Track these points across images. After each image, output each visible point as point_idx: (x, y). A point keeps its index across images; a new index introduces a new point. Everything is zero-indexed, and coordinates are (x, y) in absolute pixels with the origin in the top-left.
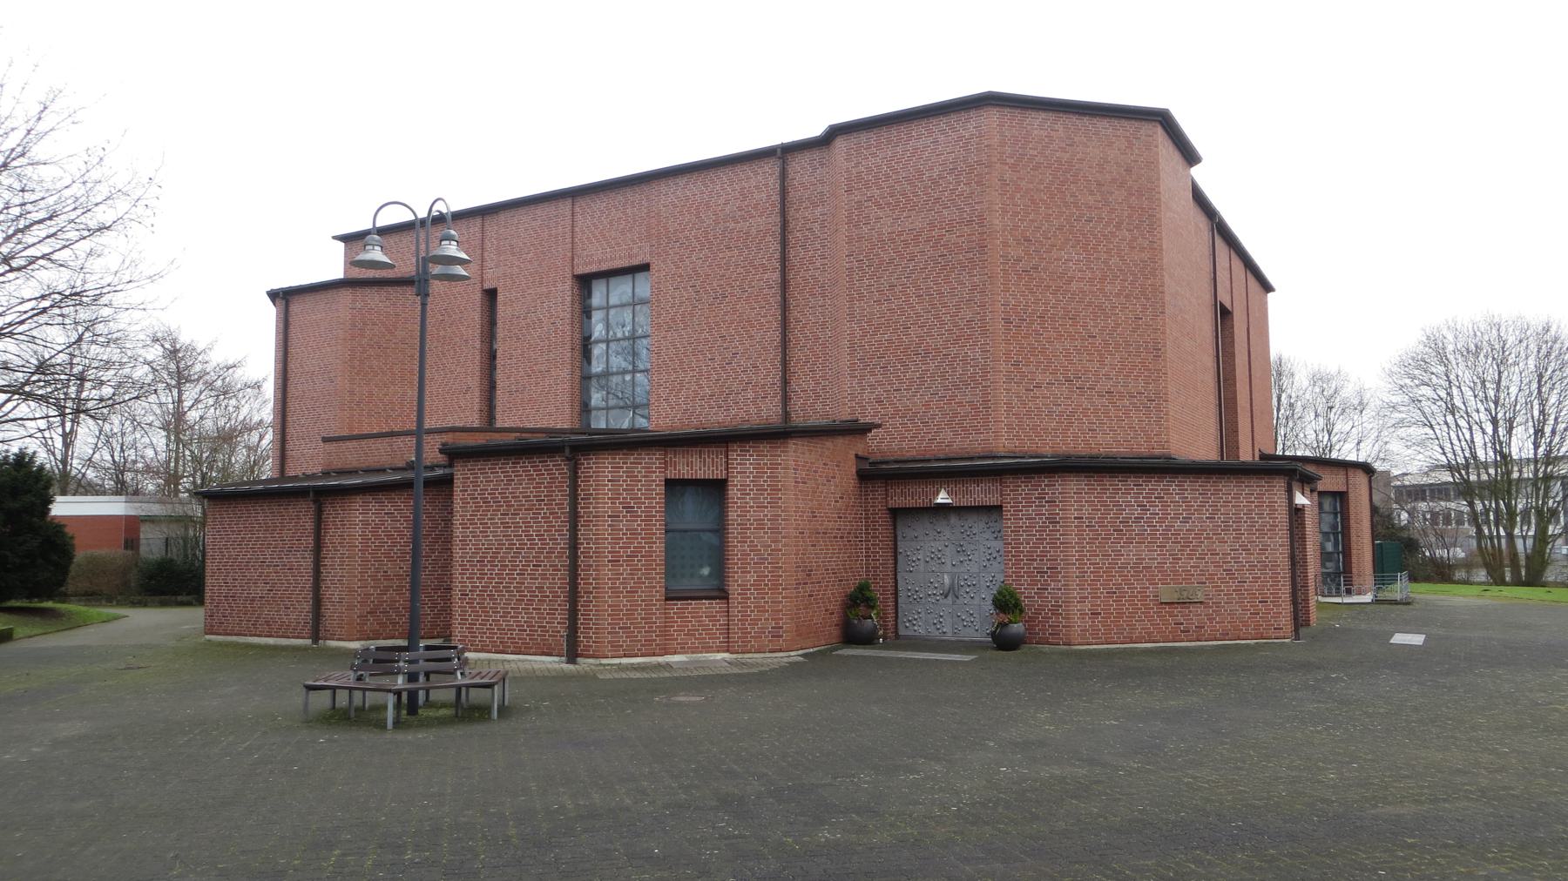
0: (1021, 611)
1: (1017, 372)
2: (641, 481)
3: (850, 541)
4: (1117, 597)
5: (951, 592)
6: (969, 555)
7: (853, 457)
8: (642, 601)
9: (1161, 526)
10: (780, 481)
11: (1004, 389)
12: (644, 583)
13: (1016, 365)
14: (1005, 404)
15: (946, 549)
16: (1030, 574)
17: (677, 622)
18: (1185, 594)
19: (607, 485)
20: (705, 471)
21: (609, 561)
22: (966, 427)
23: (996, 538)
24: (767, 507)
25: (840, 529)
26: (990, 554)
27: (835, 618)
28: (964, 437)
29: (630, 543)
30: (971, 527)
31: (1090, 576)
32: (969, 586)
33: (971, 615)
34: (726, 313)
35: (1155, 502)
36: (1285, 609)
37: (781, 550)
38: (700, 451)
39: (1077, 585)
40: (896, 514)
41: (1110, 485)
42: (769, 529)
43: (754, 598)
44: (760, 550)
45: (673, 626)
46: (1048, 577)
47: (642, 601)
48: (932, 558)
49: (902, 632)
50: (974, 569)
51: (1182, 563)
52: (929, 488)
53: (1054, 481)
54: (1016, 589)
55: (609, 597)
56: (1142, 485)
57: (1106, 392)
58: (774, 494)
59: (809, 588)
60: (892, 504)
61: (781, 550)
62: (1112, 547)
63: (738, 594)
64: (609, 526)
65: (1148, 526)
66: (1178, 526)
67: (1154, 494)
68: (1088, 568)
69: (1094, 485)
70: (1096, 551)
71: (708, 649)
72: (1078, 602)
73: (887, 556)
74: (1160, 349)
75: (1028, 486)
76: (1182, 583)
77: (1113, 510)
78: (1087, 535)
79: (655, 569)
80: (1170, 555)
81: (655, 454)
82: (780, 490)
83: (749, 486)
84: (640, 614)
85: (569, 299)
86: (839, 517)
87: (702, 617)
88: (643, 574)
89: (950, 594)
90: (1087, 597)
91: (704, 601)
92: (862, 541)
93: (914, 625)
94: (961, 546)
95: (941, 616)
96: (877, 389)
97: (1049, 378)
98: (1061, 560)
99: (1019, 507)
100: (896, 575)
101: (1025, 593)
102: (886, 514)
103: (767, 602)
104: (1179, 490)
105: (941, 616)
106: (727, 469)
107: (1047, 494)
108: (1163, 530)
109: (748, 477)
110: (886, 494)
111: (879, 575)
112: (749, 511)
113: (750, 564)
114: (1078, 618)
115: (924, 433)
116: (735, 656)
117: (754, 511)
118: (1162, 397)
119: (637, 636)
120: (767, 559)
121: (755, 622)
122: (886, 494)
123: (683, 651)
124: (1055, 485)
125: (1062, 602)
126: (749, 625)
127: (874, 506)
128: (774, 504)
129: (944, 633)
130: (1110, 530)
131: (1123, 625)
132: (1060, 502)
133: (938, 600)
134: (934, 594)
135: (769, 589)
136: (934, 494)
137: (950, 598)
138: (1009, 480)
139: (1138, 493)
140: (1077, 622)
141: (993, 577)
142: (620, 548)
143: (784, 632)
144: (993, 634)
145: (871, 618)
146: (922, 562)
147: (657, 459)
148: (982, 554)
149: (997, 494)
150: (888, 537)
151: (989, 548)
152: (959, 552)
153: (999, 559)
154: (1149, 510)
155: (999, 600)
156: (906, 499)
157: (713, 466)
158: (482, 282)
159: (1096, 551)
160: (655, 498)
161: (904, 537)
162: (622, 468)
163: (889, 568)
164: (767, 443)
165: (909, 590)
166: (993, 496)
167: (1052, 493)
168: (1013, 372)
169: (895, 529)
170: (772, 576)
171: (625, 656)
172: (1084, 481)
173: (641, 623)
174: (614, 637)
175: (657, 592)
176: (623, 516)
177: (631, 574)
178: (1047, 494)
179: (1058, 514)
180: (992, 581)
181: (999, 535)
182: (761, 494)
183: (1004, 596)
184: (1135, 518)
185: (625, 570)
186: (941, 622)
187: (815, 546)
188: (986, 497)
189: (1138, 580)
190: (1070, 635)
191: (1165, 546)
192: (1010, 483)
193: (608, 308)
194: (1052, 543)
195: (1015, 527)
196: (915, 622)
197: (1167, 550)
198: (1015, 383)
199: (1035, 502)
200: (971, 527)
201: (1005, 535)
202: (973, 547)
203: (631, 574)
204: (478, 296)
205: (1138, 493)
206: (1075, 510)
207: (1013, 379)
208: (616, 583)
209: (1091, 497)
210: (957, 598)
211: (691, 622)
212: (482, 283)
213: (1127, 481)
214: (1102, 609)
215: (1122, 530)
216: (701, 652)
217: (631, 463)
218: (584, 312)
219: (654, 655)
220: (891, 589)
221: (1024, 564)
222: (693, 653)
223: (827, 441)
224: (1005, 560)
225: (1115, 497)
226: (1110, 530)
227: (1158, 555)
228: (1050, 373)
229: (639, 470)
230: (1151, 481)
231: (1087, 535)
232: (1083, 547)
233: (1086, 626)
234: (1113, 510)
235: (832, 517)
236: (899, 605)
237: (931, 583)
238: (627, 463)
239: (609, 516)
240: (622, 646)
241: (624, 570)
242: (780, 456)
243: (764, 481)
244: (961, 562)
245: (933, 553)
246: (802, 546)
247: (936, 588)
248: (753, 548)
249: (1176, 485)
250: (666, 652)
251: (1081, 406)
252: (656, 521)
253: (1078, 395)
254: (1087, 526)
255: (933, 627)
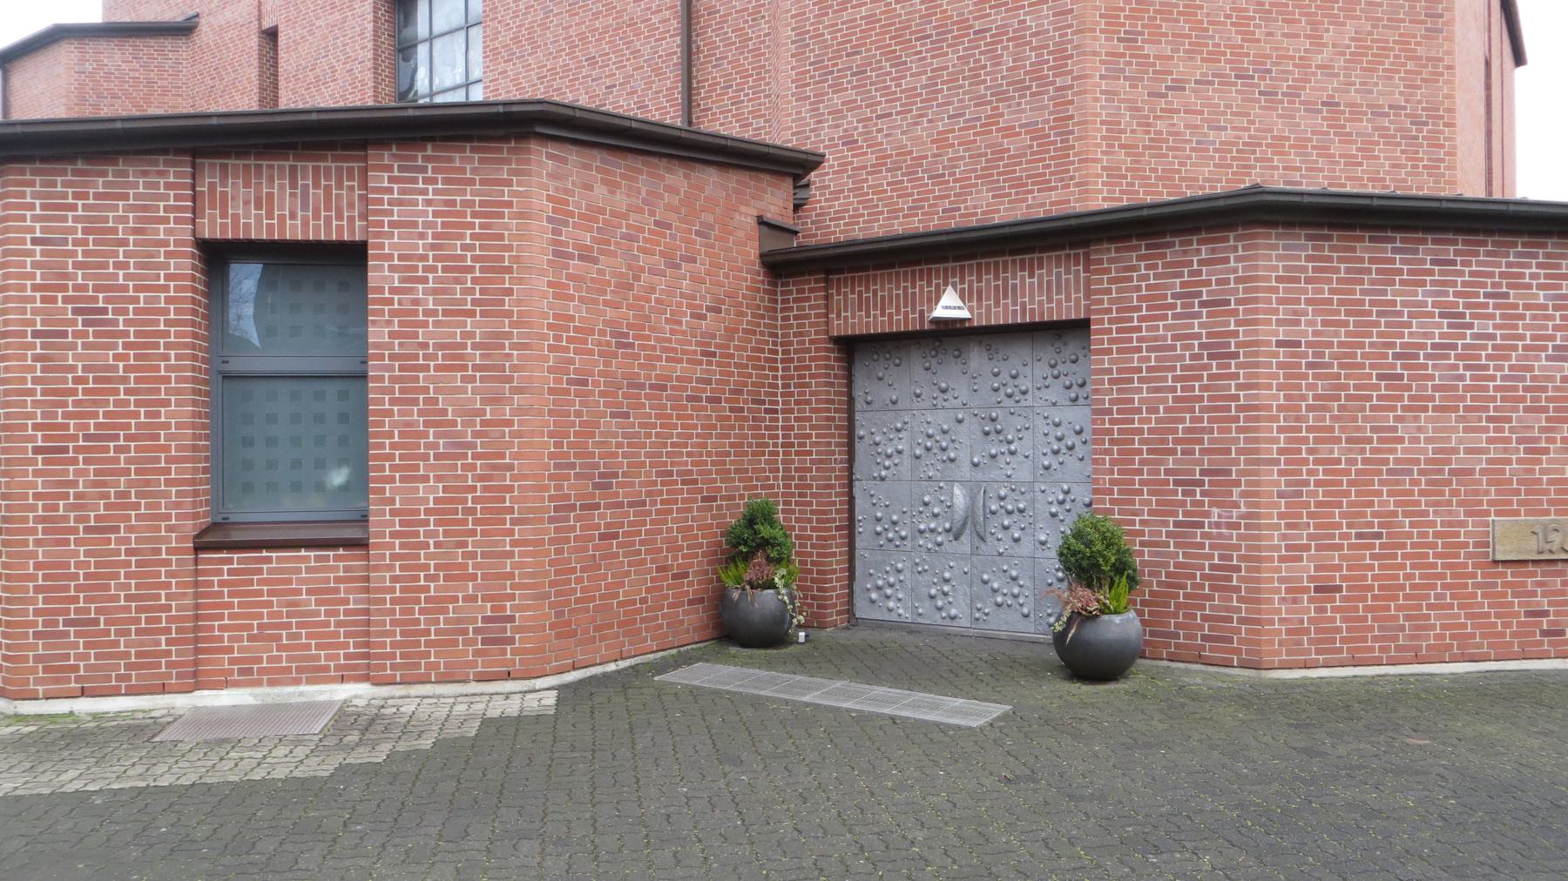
0: (1132, 581)
1: (1131, 56)
2: (124, 243)
3: (741, 410)
4: (1382, 546)
5: (968, 527)
6: (1010, 442)
7: (751, 222)
8: (129, 552)
9: (1499, 368)
10: (509, 248)
11: (1102, 92)
12: (136, 506)
13: (1130, 39)
14: (1103, 123)
15: (960, 427)
16: (1157, 487)
17: (230, 605)
18: (1557, 539)
19: (31, 253)
20: (328, 220)
21: (37, 450)
22: (1020, 178)
23: (1075, 400)
24: (471, 314)
25: (709, 382)
26: (1060, 439)
27: (692, 586)
28: (1016, 201)
29: (95, 403)
30: (1014, 377)
31: (1314, 494)
32: (1010, 513)
33: (1014, 579)
34: (596, 15)
35: (1486, 306)
36: (383, 391)
37: (510, 423)
38: (293, 170)
39: (1281, 516)
40: (851, 348)
41: (1372, 261)
42: (476, 368)
43: (438, 545)
44: (454, 423)
45: (220, 617)
46: (1204, 494)
47: (129, 552)
48: (928, 449)
49: (862, 610)
50: (1023, 474)
51: (1550, 461)
52: (921, 287)
53: (1226, 250)
54: (1119, 522)
55: (38, 543)
56: (1453, 263)
57: (1324, 104)
58: (489, 281)
59: (603, 518)
60: (839, 327)
61: (510, 423)
62: (1374, 419)
63: (394, 535)
64: (36, 358)
65: (1467, 368)
66: (1542, 368)
67: (1484, 285)
68: (1311, 472)
69: (1330, 259)
70: (1331, 429)
71: (318, 675)
72: (1282, 559)
73: (829, 444)
74: (1441, 16)
75: (1155, 267)
76: (1547, 513)
77: (1377, 324)
78: (1310, 387)
79: (167, 471)
80: (1519, 441)
81: (162, 174)
82: (509, 270)
83: (424, 258)
84: (122, 588)
85: (370, 26)
86: (704, 353)
87: (299, 592)
88: (130, 483)
89: (967, 531)
90: (1307, 548)
91: (303, 553)
92: (776, 411)
93: (888, 597)
94: (993, 420)
95: (947, 581)
96: (846, 117)
97: (1201, 70)
98: (1240, 451)
99: (1130, 340)
100: (850, 486)
101: (1142, 533)
102: (827, 350)
103: (473, 555)
104: (1547, 276)
105: (947, 581)
106: (364, 216)
107: (1208, 283)
108: (1504, 378)
109: (422, 236)
110: (827, 306)
111: (810, 487)
112: (425, 324)
113: (425, 457)
114: (1282, 600)
115: (935, 198)
116: (384, 691)
117: (437, 323)
118: (1442, 117)
119: (116, 644)
120: (472, 446)
121: (438, 605)
122: (827, 306)
123: (247, 675)
124: (1226, 260)
125: (1240, 558)
126: (422, 611)
127: (801, 334)
128: (491, 306)
129: (953, 618)
130: (1370, 376)
131: (1396, 618)
132: (1239, 302)
133: (939, 545)
134: (932, 531)
135: (477, 522)
136: (929, 300)
137: (965, 538)
138: (1107, 255)
139: (1444, 283)
140: (1278, 610)
141: (1067, 492)
142: (66, 415)
143: (516, 630)
144: (1059, 638)
145: (771, 585)
146: (906, 460)
147: (168, 186)
148: (1041, 437)
149: (1077, 291)
150: (832, 402)
151: (1057, 425)
152: (987, 434)
153: (1080, 451)
154: (1470, 326)
155: (1074, 554)
156: (868, 316)
157: (328, 209)
158: (260, 18)
159: (1331, 429)
160: (166, 289)
161: (868, 403)
162: (74, 208)
163: (833, 470)
164: (473, 150)
165: (878, 520)
166: (1068, 299)
167: (1219, 282)
168: (1123, 55)
169: (850, 385)
170: (485, 489)
171: (83, 693)
172: (1304, 248)
173: (127, 609)
174: (54, 646)
175: (170, 529)
176: (77, 334)
177: (96, 484)
178: (1208, 283)
179: (1235, 334)
180: (1062, 503)
181: (1082, 393)
182: (457, 281)
183: (1089, 544)
184: (1434, 346)
185: (81, 473)
186: (945, 594)
187: (626, 415)
188: (1050, 300)
189: (1436, 504)
190: (1258, 643)
191: (1509, 420)
192: (1111, 261)
193: (431, 39)
194: (1216, 409)
195: (1120, 371)
196: (889, 591)
197: (1512, 430)
198: (1125, 78)
199: (1173, 306)
200: (1014, 377)
201: (1096, 391)
202: (1019, 422)
203: (96, 484)
204: (253, 42)
205: (1444, 283)
206: (1280, 322)
207: (1123, 70)
208: (56, 508)
209: (1322, 291)
210: (983, 540)
211: (269, 604)
212: (259, 20)
213: (1416, 251)
214: (1343, 578)
215: (1400, 377)
216: (297, 682)
217: (97, 196)
218: (400, 51)
219: (164, 689)
220: (839, 518)
221: (1143, 462)
222: (272, 683)
223: (670, 171)
224: (1095, 452)
225: (1384, 293)
226: (1370, 376)
227: (1490, 441)
228: (1203, 60)
229: (118, 215)
230: (1477, 254)
231: (1310, 387)
232: (1298, 419)
233: (1301, 622)
234: (1377, 324)
235: (684, 352)
236: (858, 553)
237: (926, 504)
238: (85, 196)
239: (36, 334)
240: (75, 668)
241: (78, 472)
242: (509, 183)
243: (465, 247)
244: (993, 457)
245: (930, 436)
246: (578, 414)
247: (936, 516)
248: (435, 417)
249: (1539, 266)
250: (196, 680)
251: (1271, 131)
252: (168, 346)
253: (1265, 108)
254: (1310, 365)
255: (928, 603)
